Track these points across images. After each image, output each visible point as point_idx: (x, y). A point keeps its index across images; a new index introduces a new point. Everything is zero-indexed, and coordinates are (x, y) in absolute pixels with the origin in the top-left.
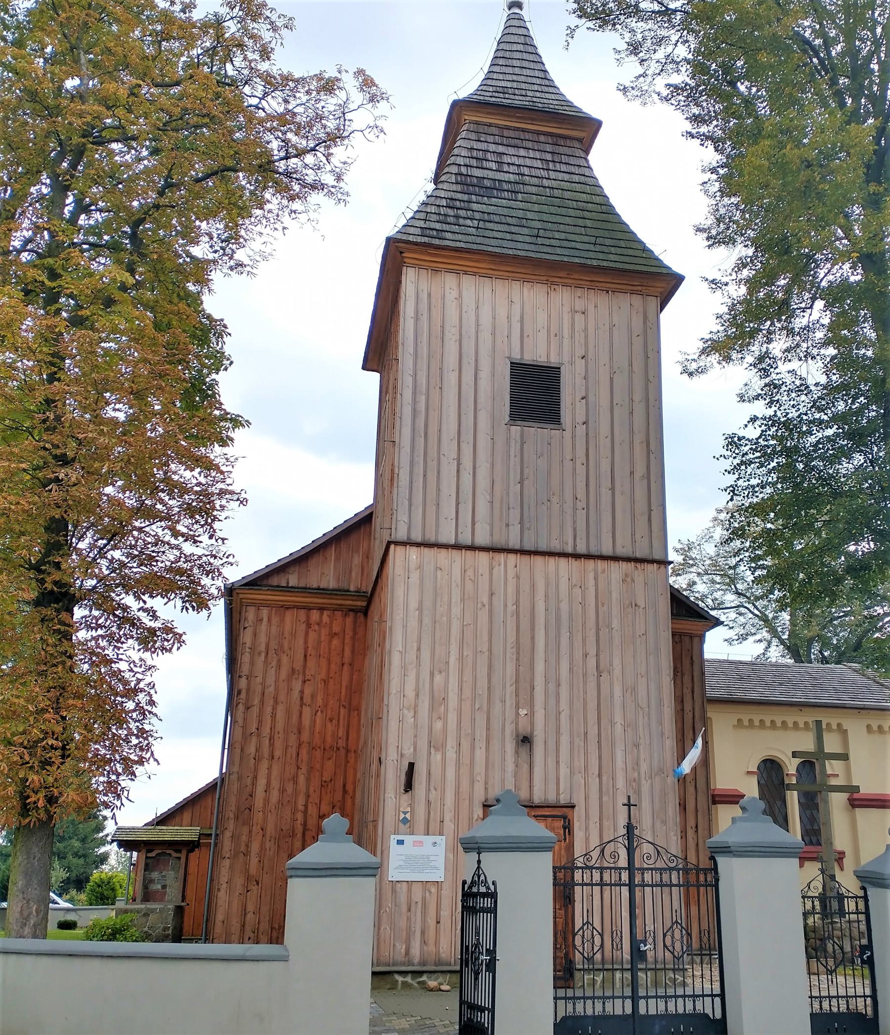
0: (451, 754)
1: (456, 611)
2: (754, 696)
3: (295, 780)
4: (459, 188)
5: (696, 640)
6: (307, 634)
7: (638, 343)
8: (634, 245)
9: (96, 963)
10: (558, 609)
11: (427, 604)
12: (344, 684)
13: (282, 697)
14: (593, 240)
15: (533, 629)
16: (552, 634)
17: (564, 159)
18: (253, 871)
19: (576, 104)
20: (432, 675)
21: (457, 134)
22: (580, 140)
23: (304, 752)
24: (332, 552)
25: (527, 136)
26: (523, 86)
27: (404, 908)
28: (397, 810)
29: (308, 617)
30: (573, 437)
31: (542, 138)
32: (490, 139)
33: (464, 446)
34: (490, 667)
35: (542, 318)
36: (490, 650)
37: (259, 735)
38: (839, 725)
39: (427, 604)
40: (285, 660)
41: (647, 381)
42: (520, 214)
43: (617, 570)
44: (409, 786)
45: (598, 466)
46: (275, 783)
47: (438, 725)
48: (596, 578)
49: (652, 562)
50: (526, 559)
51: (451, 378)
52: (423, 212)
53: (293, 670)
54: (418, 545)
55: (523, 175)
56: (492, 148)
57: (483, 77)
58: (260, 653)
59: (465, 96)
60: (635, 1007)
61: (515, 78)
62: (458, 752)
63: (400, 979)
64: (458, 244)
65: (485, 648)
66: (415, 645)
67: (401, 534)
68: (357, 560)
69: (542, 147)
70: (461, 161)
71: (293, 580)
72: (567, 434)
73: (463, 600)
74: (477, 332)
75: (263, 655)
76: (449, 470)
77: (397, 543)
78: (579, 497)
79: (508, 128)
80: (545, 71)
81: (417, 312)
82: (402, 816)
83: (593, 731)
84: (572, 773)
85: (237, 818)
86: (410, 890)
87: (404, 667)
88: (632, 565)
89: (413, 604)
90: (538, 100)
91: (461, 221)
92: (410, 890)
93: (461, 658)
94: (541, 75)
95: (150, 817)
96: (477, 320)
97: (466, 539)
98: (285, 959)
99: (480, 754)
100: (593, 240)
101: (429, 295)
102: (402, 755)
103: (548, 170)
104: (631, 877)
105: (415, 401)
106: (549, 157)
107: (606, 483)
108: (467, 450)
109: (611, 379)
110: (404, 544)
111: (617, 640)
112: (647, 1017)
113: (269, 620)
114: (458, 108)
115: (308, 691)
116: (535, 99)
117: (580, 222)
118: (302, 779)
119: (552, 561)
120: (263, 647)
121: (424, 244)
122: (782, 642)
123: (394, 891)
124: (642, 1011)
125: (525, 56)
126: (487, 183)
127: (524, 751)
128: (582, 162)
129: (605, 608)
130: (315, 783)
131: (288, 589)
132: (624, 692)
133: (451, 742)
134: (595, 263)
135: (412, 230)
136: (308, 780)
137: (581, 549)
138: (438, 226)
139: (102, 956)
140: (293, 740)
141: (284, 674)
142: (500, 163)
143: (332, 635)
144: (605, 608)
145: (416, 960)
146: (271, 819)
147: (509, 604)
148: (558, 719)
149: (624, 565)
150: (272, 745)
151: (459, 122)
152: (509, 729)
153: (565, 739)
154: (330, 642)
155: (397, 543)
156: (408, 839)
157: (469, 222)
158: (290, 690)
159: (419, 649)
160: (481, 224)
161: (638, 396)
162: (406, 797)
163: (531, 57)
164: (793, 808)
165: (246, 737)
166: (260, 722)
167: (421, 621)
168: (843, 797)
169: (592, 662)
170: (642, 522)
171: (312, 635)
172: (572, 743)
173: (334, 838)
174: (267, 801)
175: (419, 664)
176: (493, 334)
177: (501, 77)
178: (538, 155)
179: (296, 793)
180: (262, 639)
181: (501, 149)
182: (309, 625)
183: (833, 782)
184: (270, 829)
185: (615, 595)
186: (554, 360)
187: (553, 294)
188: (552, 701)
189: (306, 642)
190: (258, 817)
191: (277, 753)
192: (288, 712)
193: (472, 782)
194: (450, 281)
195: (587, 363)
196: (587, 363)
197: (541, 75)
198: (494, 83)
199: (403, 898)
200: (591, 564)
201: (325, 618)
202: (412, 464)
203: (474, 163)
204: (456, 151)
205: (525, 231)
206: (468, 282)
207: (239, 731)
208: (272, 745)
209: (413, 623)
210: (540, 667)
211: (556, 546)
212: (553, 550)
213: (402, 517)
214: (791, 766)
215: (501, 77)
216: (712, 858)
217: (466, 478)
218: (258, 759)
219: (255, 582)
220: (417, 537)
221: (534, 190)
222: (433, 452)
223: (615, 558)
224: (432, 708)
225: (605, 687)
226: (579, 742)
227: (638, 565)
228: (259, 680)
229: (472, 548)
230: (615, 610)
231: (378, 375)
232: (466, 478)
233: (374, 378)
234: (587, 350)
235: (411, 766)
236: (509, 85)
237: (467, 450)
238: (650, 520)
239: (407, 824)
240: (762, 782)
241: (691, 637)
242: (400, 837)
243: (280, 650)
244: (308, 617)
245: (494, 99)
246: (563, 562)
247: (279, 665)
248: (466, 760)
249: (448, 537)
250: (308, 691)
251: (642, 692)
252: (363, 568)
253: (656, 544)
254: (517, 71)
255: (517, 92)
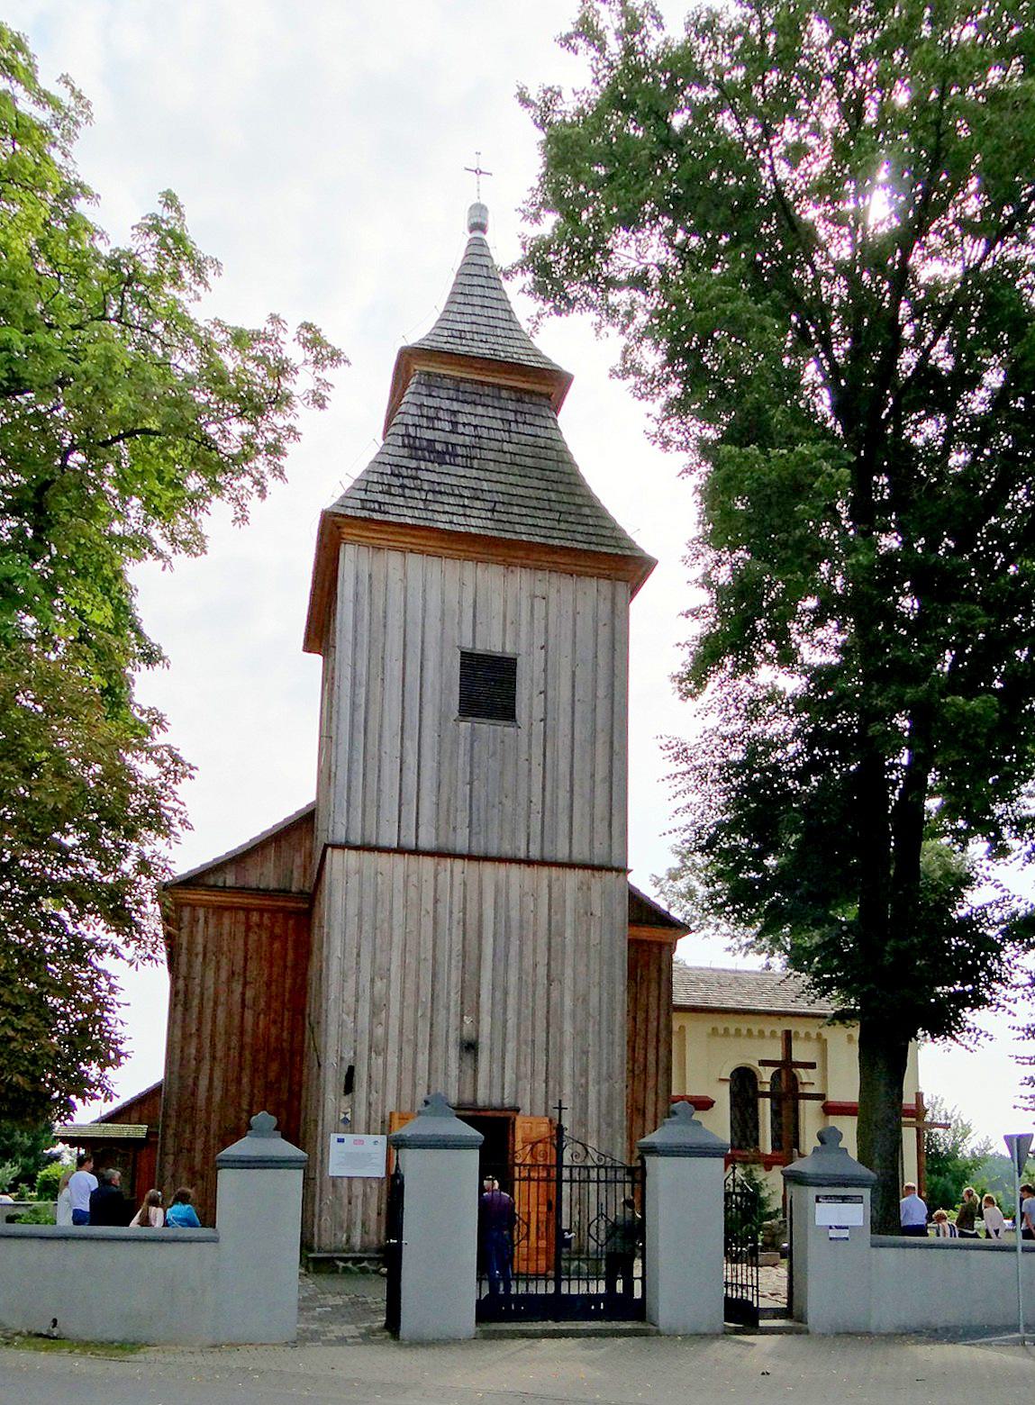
0: (393, 1059)
1: (398, 917)
2: (731, 1004)
3: (239, 1081)
4: (405, 452)
5: (667, 948)
6: (247, 936)
7: (604, 633)
8: (602, 523)
9: (35, 1244)
10: (508, 918)
11: (368, 910)
12: (287, 986)
13: (222, 999)
14: (557, 516)
15: (480, 936)
16: (501, 942)
17: (529, 419)
18: (198, 1167)
19: (544, 353)
20: (372, 981)
21: (406, 386)
22: (548, 397)
23: (247, 1054)
24: (271, 851)
25: (487, 390)
26: (484, 329)
27: (346, 1201)
28: (338, 1110)
29: (247, 918)
30: (530, 735)
31: (504, 394)
32: (443, 394)
33: (408, 744)
34: (434, 975)
35: (497, 605)
36: (434, 957)
37: (199, 1036)
38: (819, 1035)
39: (368, 910)
40: (224, 961)
41: (613, 675)
42: (473, 484)
43: (572, 878)
44: (349, 1088)
45: (556, 766)
46: (217, 1083)
47: (380, 1031)
48: (550, 887)
49: (610, 869)
50: (474, 865)
51: (394, 668)
52: (364, 484)
53: (233, 973)
54: (357, 848)
55: (480, 437)
56: (446, 404)
57: (438, 317)
58: (197, 955)
59: (416, 340)
60: (558, 1287)
61: (474, 319)
62: (400, 1058)
63: (341, 1264)
64: (402, 520)
65: (429, 955)
66: (355, 950)
67: (340, 837)
68: (298, 861)
69: (503, 404)
70: (409, 420)
71: (230, 880)
72: (523, 733)
73: (405, 906)
74: (424, 618)
75: (200, 957)
76: (390, 769)
77: (334, 846)
78: (534, 799)
79: (463, 380)
80: (510, 312)
81: (356, 595)
82: (342, 1116)
83: (541, 1036)
84: (518, 1078)
85: (179, 1116)
86: (350, 1186)
87: (344, 974)
88: (588, 873)
89: (352, 910)
90: (500, 348)
91: (408, 492)
92: (350, 1186)
93: (404, 965)
94: (506, 316)
95: (97, 1117)
96: (424, 606)
97: (409, 841)
98: (215, 1240)
99: (423, 1059)
100: (557, 516)
101: (370, 576)
102: (342, 1059)
103: (510, 431)
104: (560, 1174)
105: (354, 694)
106: (511, 416)
107: (564, 785)
108: (411, 746)
109: (574, 673)
110: (347, 846)
111: (569, 950)
112: (569, 1296)
113: (206, 922)
114: (408, 358)
115: (249, 994)
116: (496, 347)
117: (545, 495)
118: (245, 1080)
119: (502, 868)
120: (200, 949)
121: (365, 519)
122: (786, 952)
123: (334, 1185)
124: (564, 1291)
125: (488, 292)
126: (439, 447)
127: (468, 1059)
128: (550, 423)
129: (559, 917)
130: (260, 1083)
131: (224, 888)
132: (575, 1000)
133: (393, 1047)
134: (556, 542)
135: (350, 503)
136: (252, 1082)
137: (535, 853)
138: (380, 498)
139: (41, 1238)
140: (234, 1041)
141: (224, 975)
142: (455, 424)
143: (273, 937)
144: (559, 917)
145: (358, 1247)
146: (215, 1117)
147: (456, 910)
148: (505, 1027)
149: (579, 873)
150: (213, 1046)
151: (407, 371)
152: (453, 1037)
153: (511, 1046)
154: (271, 944)
155: (334, 846)
156: (348, 1137)
157: (416, 494)
158: (230, 992)
159: (358, 955)
160: (430, 497)
161: (601, 692)
162: (347, 1098)
163: (494, 294)
164: (764, 1114)
165: (186, 1037)
166: (200, 1023)
167: (360, 928)
168: (817, 1104)
169: (542, 971)
170: (601, 828)
171: (253, 937)
172: (518, 1050)
173: (261, 1134)
174: (209, 1099)
175: (358, 970)
176: (442, 620)
177: (458, 318)
178: (498, 414)
179: (240, 1093)
180: (200, 939)
181: (456, 406)
182: (248, 928)
183: (809, 1090)
184: (214, 1126)
185: (569, 904)
186: (510, 650)
187: (510, 576)
188: (499, 1009)
189: (246, 944)
190: (202, 1115)
191: (219, 1054)
192: (230, 1014)
193: (414, 1085)
194: (394, 559)
195: (547, 652)
196: (547, 652)
197: (506, 316)
198: (449, 325)
199: (344, 1192)
200: (545, 871)
201: (266, 921)
202: (351, 761)
203: (424, 422)
204: (403, 408)
205: (478, 504)
206: (414, 560)
207: (178, 1033)
208: (213, 1046)
209: (352, 929)
210: (486, 976)
211: (507, 849)
212: (504, 856)
213: (341, 820)
214: (766, 1074)
215: (458, 318)
216: (641, 1158)
217: (411, 777)
218: (199, 1060)
219: (195, 881)
220: (356, 839)
221: (491, 455)
222: (373, 749)
223: (571, 865)
224: (373, 1014)
225: (555, 994)
226: (527, 1050)
227: (596, 874)
228: (197, 981)
229: (416, 852)
230: (569, 918)
231: (320, 658)
232: (411, 777)
233: (317, 660)
234: (546, 641)
235: (351, 1069)
236: (467, 328)
237: (411, 746)
238: (610, 825)
239: (349, 1125)
240: (735, 1089)
241: (661, 945)
242: (341, 1136)
243: (219, 951)
244: (247, 918)
245: (448, 346)
246: (514, 868)
247: (218, 969)
248: (408, 1064)
249: (389, 839)
250: (249, 994)
251: (594, 1000)
252: (305, 869)
253: (616, 851)
254: (478, 310)
255: (476, 337)
